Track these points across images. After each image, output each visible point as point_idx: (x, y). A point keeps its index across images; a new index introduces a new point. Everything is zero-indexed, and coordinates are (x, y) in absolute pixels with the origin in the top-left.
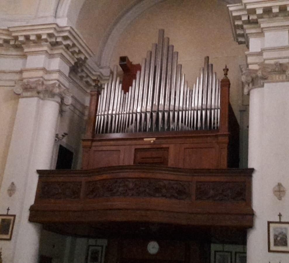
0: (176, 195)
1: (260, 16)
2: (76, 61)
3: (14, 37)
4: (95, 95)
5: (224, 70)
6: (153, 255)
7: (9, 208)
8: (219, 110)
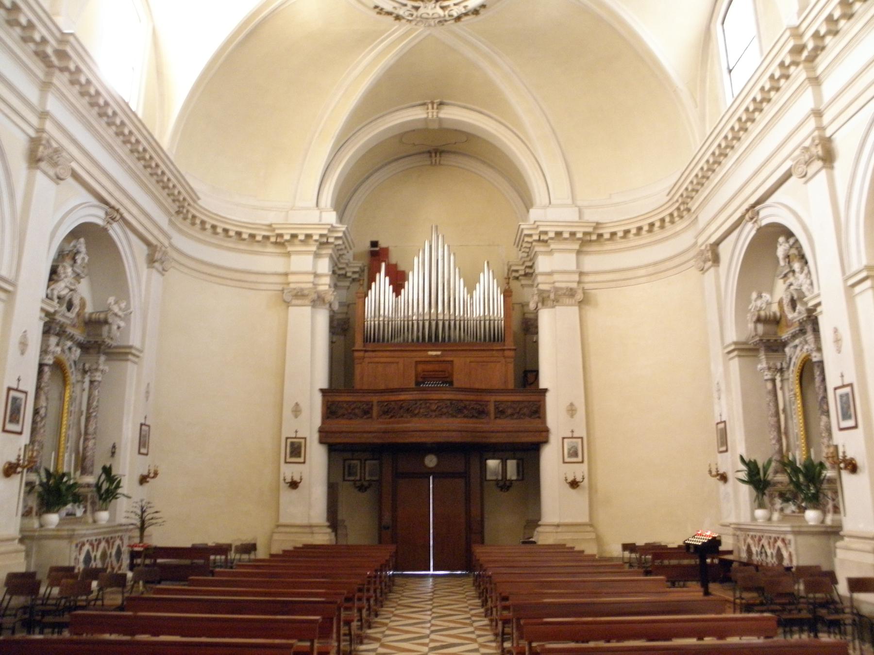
6: (432, 468)
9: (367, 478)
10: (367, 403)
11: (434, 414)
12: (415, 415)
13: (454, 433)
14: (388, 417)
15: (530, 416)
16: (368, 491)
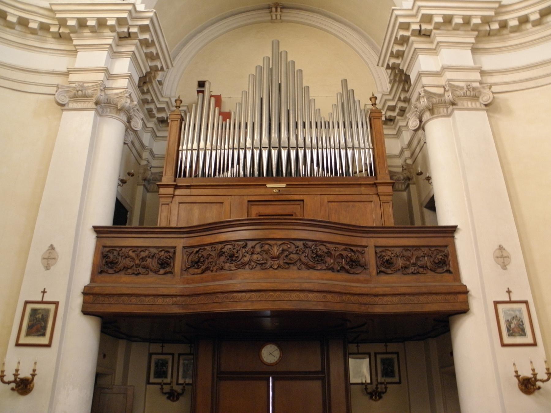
1: (438, 26)
2: (149, 70)
3: (59, 19)
4: (177, 121)
5: (371, 99)
7: (45, 289)
8: (371, 150)
9: (181, 381)
11: (276, 264)
12: (244, 265)
13: (311, 295)
15: (433, 270)
16: (181, 398)
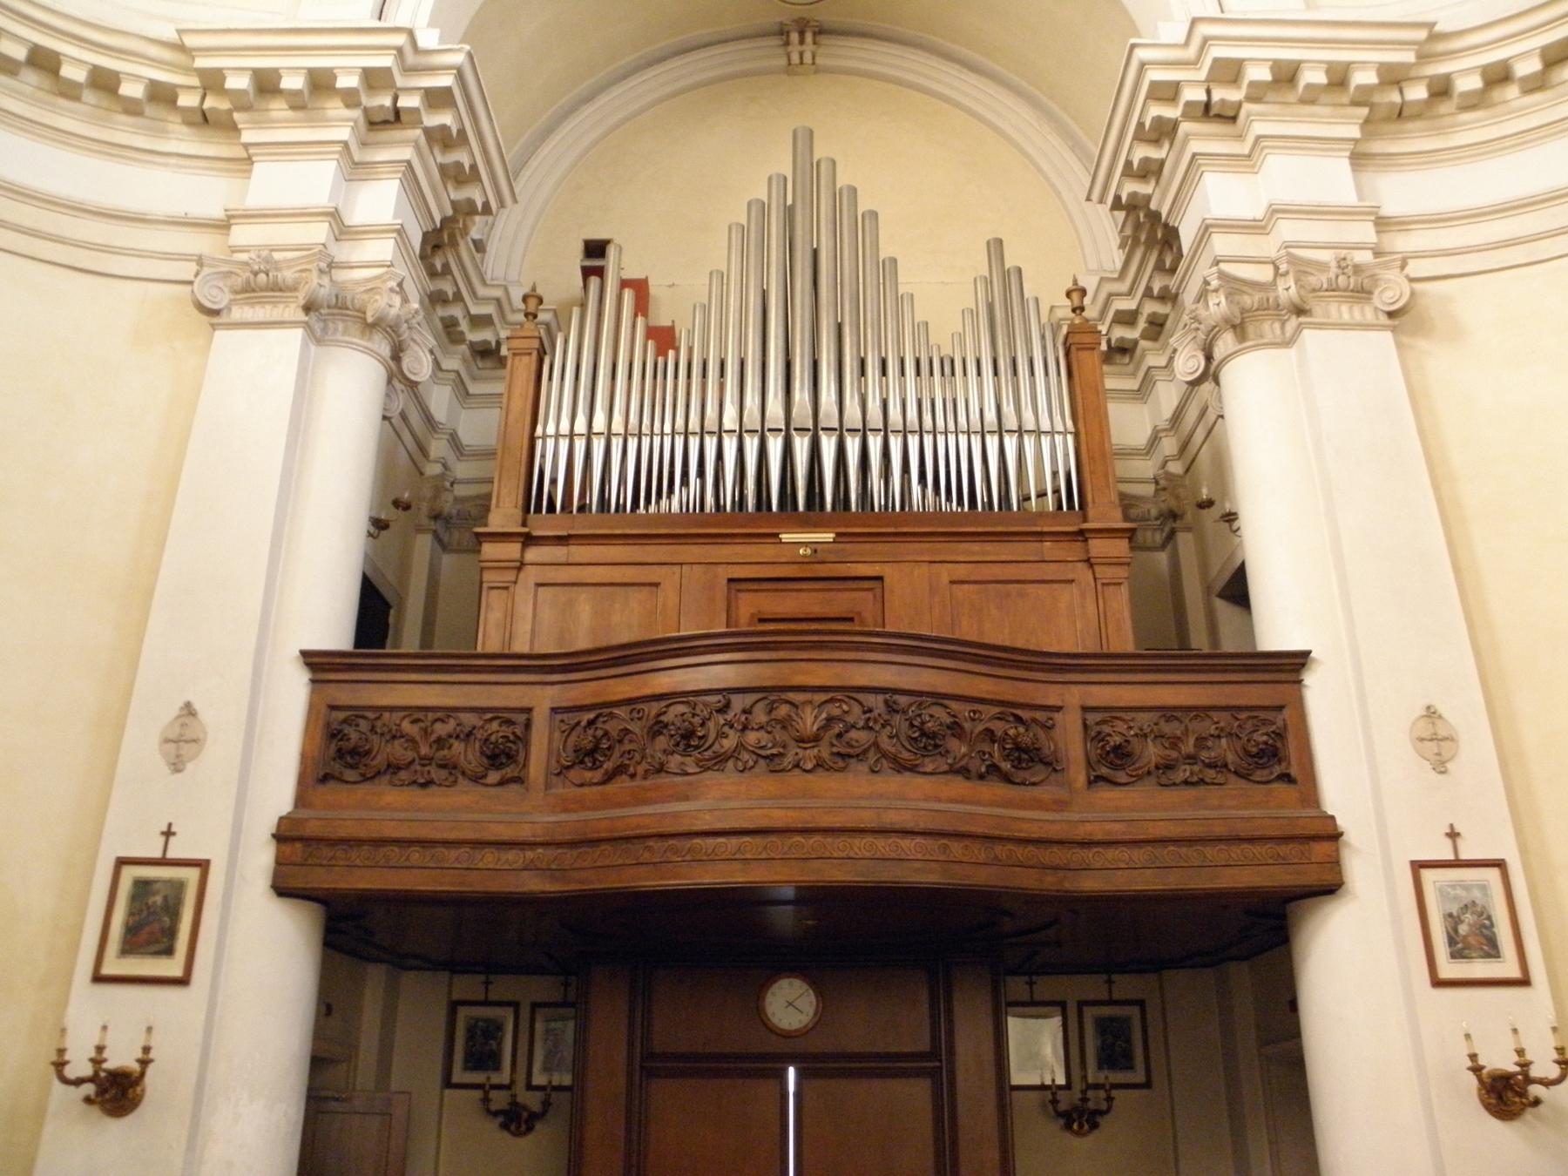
0: (1006, 766)
1: (1257, 93)
2: (450, 212)
4: (530, 354)
6: (787, 1035)
7: (170, 825)
9: (539, 1079)
10: (501, 715)
12: (720, 760)
13: (906, 843)
14: (598, 775)
